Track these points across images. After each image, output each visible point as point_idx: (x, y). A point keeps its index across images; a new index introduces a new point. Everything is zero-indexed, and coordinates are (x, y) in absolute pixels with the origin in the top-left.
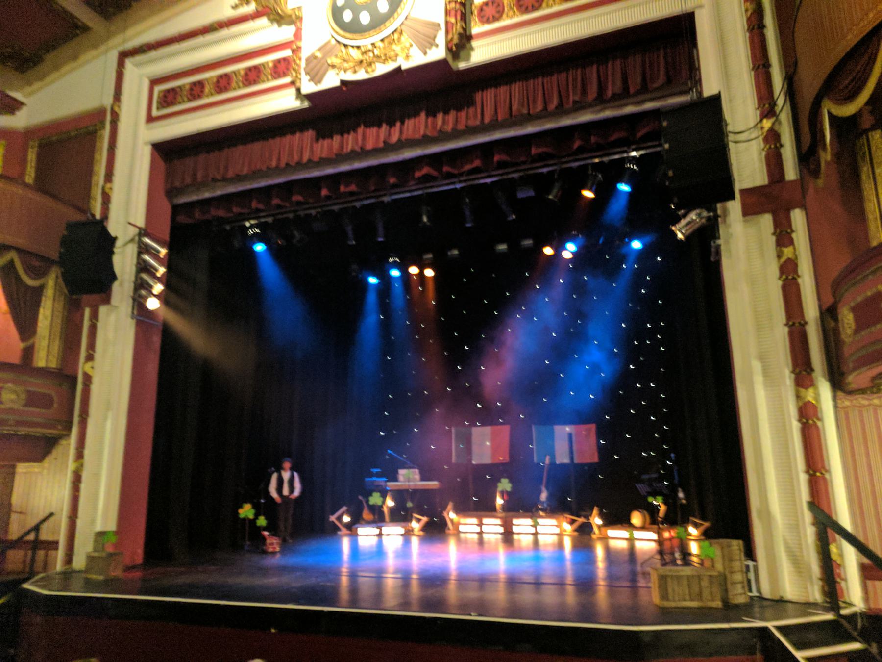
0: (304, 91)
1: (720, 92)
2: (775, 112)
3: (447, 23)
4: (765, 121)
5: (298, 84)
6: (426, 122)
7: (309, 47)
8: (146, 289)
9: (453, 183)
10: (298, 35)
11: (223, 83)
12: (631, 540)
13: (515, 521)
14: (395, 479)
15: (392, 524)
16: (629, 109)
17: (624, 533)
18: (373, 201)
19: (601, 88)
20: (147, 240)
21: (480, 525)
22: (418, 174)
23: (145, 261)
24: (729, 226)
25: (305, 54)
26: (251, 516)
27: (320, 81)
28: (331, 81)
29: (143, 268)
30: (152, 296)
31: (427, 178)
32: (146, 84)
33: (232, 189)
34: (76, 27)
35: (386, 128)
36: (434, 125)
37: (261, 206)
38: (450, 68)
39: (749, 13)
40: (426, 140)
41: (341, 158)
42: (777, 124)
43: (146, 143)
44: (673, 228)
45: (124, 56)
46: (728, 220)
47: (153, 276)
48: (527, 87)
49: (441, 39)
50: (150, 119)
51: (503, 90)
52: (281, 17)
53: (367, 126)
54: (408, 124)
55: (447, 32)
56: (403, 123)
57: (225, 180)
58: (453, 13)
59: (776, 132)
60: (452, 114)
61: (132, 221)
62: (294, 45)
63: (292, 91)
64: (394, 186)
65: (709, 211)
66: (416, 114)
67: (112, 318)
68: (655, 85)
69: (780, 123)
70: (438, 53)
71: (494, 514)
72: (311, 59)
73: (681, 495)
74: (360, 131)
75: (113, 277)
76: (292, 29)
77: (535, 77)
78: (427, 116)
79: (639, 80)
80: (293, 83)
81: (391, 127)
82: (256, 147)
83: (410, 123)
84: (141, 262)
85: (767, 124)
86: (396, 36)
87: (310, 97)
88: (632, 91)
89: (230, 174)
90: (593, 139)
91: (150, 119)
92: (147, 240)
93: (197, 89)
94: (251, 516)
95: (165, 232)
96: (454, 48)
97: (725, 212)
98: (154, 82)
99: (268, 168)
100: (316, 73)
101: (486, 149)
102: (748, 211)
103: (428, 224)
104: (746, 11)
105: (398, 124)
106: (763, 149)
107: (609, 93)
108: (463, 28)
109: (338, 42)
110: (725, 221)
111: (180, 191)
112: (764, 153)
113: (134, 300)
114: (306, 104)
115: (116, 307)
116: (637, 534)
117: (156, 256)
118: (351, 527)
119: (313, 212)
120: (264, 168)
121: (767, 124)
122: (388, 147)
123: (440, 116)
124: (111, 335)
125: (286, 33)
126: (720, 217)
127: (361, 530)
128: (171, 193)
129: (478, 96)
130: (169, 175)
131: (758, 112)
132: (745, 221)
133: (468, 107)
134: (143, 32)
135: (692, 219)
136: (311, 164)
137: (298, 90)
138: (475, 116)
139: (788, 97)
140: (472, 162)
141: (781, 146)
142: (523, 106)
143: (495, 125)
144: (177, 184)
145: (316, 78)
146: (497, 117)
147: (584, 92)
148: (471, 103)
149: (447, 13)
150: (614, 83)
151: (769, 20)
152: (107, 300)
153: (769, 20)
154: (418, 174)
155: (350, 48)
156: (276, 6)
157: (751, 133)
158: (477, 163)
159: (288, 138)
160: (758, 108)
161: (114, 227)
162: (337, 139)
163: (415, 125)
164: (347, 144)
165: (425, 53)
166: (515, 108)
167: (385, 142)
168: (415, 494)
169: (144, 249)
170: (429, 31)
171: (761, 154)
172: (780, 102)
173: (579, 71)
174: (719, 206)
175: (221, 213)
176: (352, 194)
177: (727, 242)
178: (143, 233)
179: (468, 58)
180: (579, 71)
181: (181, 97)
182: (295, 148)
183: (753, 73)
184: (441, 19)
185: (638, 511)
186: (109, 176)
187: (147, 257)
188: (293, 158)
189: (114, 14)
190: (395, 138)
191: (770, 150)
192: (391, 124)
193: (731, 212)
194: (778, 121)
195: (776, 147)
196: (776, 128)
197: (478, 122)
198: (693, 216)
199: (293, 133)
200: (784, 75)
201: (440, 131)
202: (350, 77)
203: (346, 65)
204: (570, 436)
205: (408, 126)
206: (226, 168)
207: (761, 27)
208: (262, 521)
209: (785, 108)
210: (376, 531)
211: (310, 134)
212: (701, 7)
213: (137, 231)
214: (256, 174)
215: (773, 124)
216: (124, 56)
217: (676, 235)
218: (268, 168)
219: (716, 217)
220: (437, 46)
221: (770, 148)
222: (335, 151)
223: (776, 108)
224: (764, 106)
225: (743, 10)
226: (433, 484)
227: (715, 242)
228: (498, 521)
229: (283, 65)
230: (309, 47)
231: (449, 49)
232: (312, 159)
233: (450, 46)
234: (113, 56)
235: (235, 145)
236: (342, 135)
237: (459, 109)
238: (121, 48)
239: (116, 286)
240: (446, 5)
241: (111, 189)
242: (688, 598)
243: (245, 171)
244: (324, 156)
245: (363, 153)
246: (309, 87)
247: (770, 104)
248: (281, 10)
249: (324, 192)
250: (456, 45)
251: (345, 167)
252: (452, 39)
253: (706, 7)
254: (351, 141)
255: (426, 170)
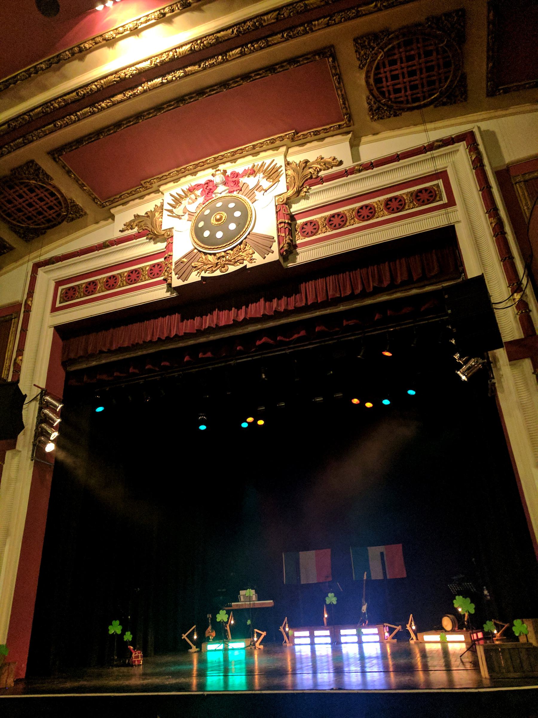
0: (174, 285)
1: (483, 274)
2: (522, 288)
3: (278, 236)
4: (515, 294)
5: (169, 281)
6: (265, 305)
7: (178, 254)
8: (44, 436)
9: (284, 350)
10: (169, 247)
11: (111, 282)
12: (444, 643)
13: (343, 632)
14: (237, 600)
15: (233, 640)
16: (414, 292)
17: (436, 637)
18: (223, 364)
19: (393, 278)
20: (48, 398)
21: (312, 636)
22: (258, 343)
23: (46, 415)
24: (499, 369)
25: (175, 259)
26: (119, 632)
27: (186, 279)
28: (194, 277)
29: (43, 419)
30: (50, 442)
31: (265, 346)
32: (53, 285)
33: (114, 359)
34: (5, 247)
35: (234, 312)
36: (271, 307)
37: (137, 371)
38: (282, 266)
39: (494, 225)
40: (265, 318)
41: (200, 333)
42: (524, 296)
43: (50, 327)
44: (458, 372)
45: (37, 266)
46: (498, 364)
47: (51, 425)
48: (338, 279)
49: (275, 247)
50: (54, 309)
51: (320, 282)
52: (157, 236)
53: (220, 309)
54: (251, 306)
55: (279, 244)
56: (247, 307)
57: (111, 352)
58: (283, 230)
59: (524, 301)
60: (284, 299)
61: (37, 384)
62: (166, 254)
63: (165, 285)
64: (240, 353)
65: (483, 359)
66: (257, 300)
67: (16, 460)
68: (433, 274)
69: (526, 296)
70: (274, 256)
71: (322, 627)
72: (179, 262)
73: (486, 592)
74: (215, 313)
75: (21, 427)
76: (164, 244)
77: (344, 272)
78: (266, 301)
79: (420, 271)
80: (165, 280)
81: (238, 310)
82: (136, 327)
83: (252, 307)
84: (42, 415)
85: (517, 296)
86: (242, 246)
87: (177, 289)
88: (415, 278)
89: (114, 348)
90: (389, 313)
91: (54, 309)
92: (48, 398)
93: (91, 287)
94: (119, 632)
95: (60, 392)
96: (285, 253)
97: (496, 360)
98: (59, 283)
99: (144, 342)
100: (182, 275)
101: (308, 324)
102: (513, 358)
103: (266, 379)
104: (491, 223)
105: (244, 307)
106: (517, 314)
107: (399, 281)
108: (290, 239)
109: (200, 251)
110: (496, 366)
111: (73, 362)
112: (518, 317)
113: (34, 445)
114: (175, 295)
115: (20, 451)
116: (450, 637)
117: (54, 411)
118: (199, 644)
119: (176, 374)
120: (141, 342)
121: (517, 296)
122: (236, 324)
123: (275, 301)
124: (13, 475)
125: (161, 246)
126: (492, 363)
127: (211, 647)
128: (65, 364)
129: (303, 286)
130: (65, 350)
131: (510, 289)
132: (510, 365)
133: (296, 294)
134: (55, 248)
135: (471, 365)
136: (177, 338)
137: (170, 285)
138: (301, 300)
139: (529, 279)
140: (299, 333)
141: (530, 311)
142: (336, 292)
143: (315, 306)
144: (72, 356)
145: (182, 275)
146: (318, 301)
147: (381, 281)
148: (297, 291)
149: (278, 230)
150: (401, 275)
151: (508, 229)
152: (13, 446)
153: (508, 229)
154: (258, 343)
155: (209, 256)
156: (153, 229)
157: (507, 303)
158: (303, 333)
159: (160, 319)
160: (509, 287)
161: (24, 387)
162: (197, 319)
163: (256, 307)
164: (206, 323)
165: (264, 258)
166: (330, 293)
167: (233, 320)
168: (253, 612)
169: (44, 405)
170: (267, 243)
171: (515, 317)
172: (524, 281)
173: (375, 267)
174: (490, 353)
175: (104, 377)
176: (208, 359)
177: (500, 382)
178: (44, 393)
179: (294, 260)
180: (375, 267)
181: (79, 293)
182: (165, 327)
183: (502, 263)
184: (274, 233)
185: (446, 616)
186: (21, 351)
187: (47, 411)
188: (163, 333)
189: (33, 238)
190: (241, 318)
191: (522, 314)
192: (239, 308)
193: (500, 360)
194: (524, 294)
195: (526, 312)
196: (524, 299)
197: (304, 304)
198: (472, 362)
199: (164, 316)
200: (524, 265)
201: (275, 311)
202: (207, 275)
203: (206, 267)
204: (382, 554)
205: (251, 309)
206: (111, 343)
207: (504, 233)
208: (128, 637)
209: (528, 286)
210: (221, 646)
211: (176, 317)
212: (458, 222)
213: (40, 390)
214: (135, 347)
215: (522, 297)
216: (37, 266)
217: (460, 378)
218: (144, 342)
219: (489, 363)
220: (273, 252)
221: (522, 312)
222: (196, 328)
223: (522, 286)
224: (514, 284)
225: (489, 223)
226: (269, 603)
227: (491, 381)
228: (327, 633)
229: (157, 268)
230: (178, 254)
231: (281, 254)
232: (178, 333)
233: (281, 251)
234: (31, 264)
235: (120, 326)
236: (202, 317)
237: (289, 296)
238: (37, 260)
239: (20, 437)
240: (278, 225)
241: (21, 360)
242: (511, 669)
243: (126, 344)
244: (187, 332)
245: (218, 329)
246: (176, 282)
247: (517, 283)
248: (157, 231)
249: (187, 359)
250: (286, 251)
251: (202, 340)
252: (282, 248)
253: (462, 221)
254: (208, 321)
255: (264, 340)
